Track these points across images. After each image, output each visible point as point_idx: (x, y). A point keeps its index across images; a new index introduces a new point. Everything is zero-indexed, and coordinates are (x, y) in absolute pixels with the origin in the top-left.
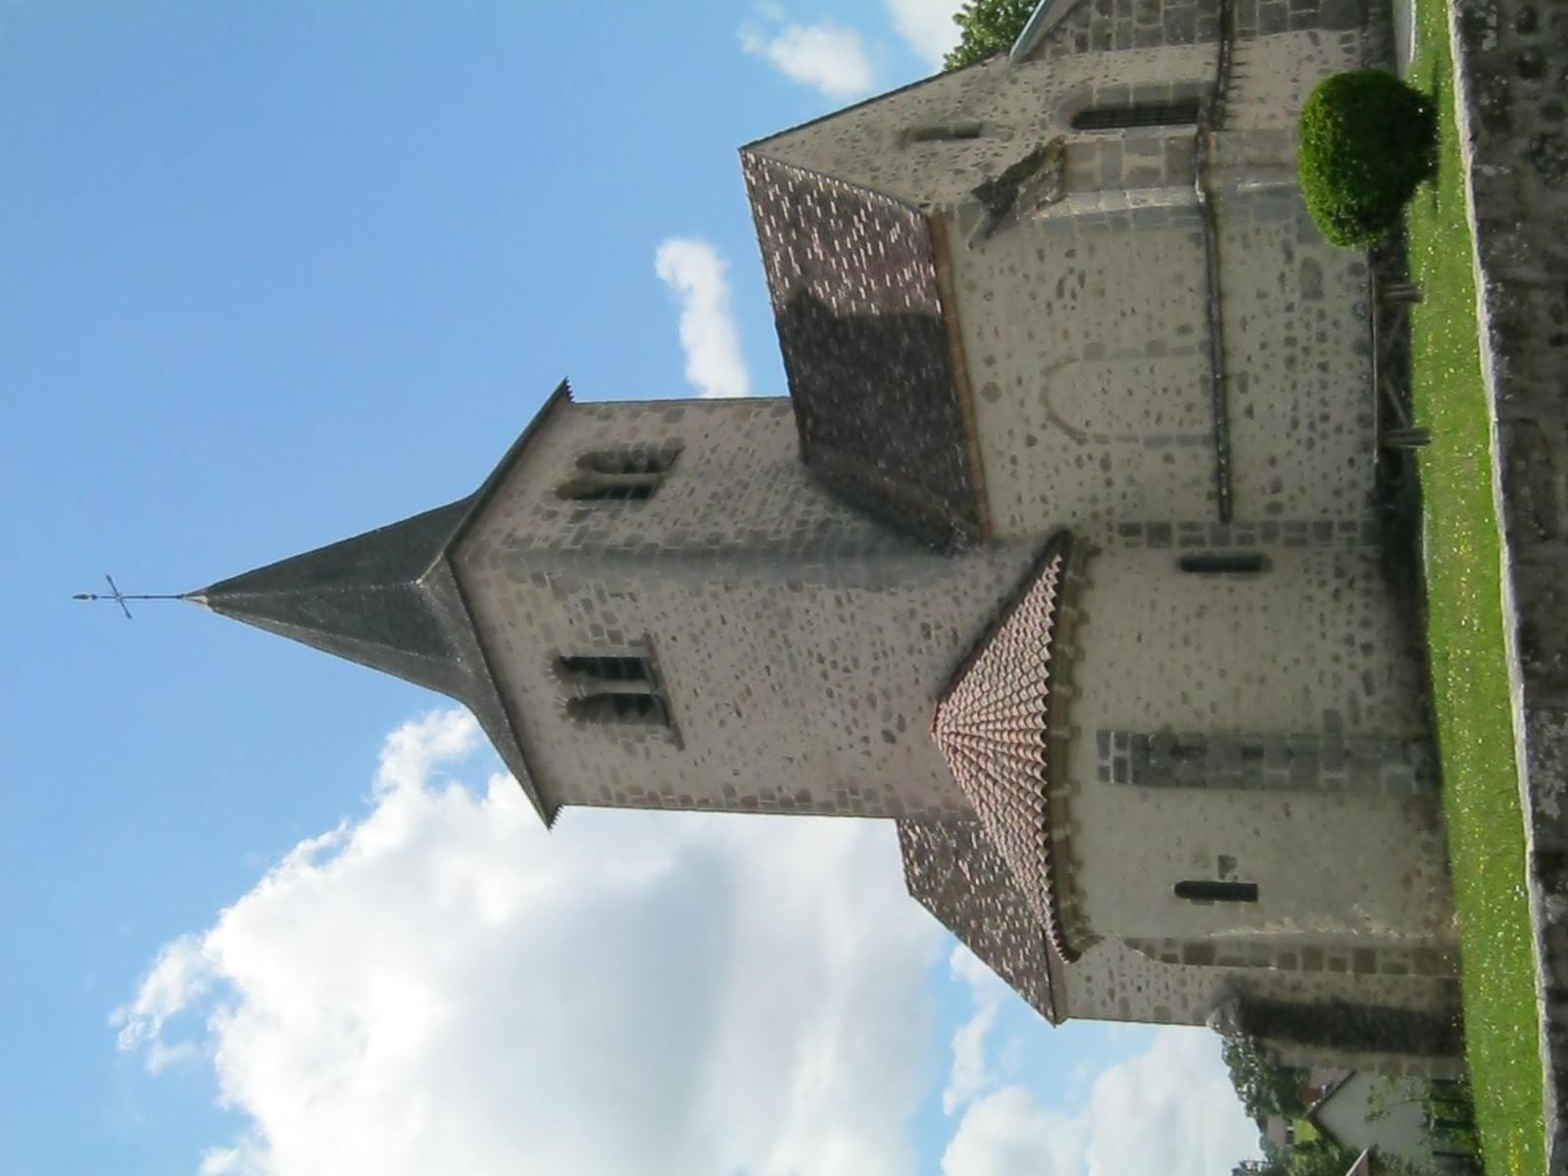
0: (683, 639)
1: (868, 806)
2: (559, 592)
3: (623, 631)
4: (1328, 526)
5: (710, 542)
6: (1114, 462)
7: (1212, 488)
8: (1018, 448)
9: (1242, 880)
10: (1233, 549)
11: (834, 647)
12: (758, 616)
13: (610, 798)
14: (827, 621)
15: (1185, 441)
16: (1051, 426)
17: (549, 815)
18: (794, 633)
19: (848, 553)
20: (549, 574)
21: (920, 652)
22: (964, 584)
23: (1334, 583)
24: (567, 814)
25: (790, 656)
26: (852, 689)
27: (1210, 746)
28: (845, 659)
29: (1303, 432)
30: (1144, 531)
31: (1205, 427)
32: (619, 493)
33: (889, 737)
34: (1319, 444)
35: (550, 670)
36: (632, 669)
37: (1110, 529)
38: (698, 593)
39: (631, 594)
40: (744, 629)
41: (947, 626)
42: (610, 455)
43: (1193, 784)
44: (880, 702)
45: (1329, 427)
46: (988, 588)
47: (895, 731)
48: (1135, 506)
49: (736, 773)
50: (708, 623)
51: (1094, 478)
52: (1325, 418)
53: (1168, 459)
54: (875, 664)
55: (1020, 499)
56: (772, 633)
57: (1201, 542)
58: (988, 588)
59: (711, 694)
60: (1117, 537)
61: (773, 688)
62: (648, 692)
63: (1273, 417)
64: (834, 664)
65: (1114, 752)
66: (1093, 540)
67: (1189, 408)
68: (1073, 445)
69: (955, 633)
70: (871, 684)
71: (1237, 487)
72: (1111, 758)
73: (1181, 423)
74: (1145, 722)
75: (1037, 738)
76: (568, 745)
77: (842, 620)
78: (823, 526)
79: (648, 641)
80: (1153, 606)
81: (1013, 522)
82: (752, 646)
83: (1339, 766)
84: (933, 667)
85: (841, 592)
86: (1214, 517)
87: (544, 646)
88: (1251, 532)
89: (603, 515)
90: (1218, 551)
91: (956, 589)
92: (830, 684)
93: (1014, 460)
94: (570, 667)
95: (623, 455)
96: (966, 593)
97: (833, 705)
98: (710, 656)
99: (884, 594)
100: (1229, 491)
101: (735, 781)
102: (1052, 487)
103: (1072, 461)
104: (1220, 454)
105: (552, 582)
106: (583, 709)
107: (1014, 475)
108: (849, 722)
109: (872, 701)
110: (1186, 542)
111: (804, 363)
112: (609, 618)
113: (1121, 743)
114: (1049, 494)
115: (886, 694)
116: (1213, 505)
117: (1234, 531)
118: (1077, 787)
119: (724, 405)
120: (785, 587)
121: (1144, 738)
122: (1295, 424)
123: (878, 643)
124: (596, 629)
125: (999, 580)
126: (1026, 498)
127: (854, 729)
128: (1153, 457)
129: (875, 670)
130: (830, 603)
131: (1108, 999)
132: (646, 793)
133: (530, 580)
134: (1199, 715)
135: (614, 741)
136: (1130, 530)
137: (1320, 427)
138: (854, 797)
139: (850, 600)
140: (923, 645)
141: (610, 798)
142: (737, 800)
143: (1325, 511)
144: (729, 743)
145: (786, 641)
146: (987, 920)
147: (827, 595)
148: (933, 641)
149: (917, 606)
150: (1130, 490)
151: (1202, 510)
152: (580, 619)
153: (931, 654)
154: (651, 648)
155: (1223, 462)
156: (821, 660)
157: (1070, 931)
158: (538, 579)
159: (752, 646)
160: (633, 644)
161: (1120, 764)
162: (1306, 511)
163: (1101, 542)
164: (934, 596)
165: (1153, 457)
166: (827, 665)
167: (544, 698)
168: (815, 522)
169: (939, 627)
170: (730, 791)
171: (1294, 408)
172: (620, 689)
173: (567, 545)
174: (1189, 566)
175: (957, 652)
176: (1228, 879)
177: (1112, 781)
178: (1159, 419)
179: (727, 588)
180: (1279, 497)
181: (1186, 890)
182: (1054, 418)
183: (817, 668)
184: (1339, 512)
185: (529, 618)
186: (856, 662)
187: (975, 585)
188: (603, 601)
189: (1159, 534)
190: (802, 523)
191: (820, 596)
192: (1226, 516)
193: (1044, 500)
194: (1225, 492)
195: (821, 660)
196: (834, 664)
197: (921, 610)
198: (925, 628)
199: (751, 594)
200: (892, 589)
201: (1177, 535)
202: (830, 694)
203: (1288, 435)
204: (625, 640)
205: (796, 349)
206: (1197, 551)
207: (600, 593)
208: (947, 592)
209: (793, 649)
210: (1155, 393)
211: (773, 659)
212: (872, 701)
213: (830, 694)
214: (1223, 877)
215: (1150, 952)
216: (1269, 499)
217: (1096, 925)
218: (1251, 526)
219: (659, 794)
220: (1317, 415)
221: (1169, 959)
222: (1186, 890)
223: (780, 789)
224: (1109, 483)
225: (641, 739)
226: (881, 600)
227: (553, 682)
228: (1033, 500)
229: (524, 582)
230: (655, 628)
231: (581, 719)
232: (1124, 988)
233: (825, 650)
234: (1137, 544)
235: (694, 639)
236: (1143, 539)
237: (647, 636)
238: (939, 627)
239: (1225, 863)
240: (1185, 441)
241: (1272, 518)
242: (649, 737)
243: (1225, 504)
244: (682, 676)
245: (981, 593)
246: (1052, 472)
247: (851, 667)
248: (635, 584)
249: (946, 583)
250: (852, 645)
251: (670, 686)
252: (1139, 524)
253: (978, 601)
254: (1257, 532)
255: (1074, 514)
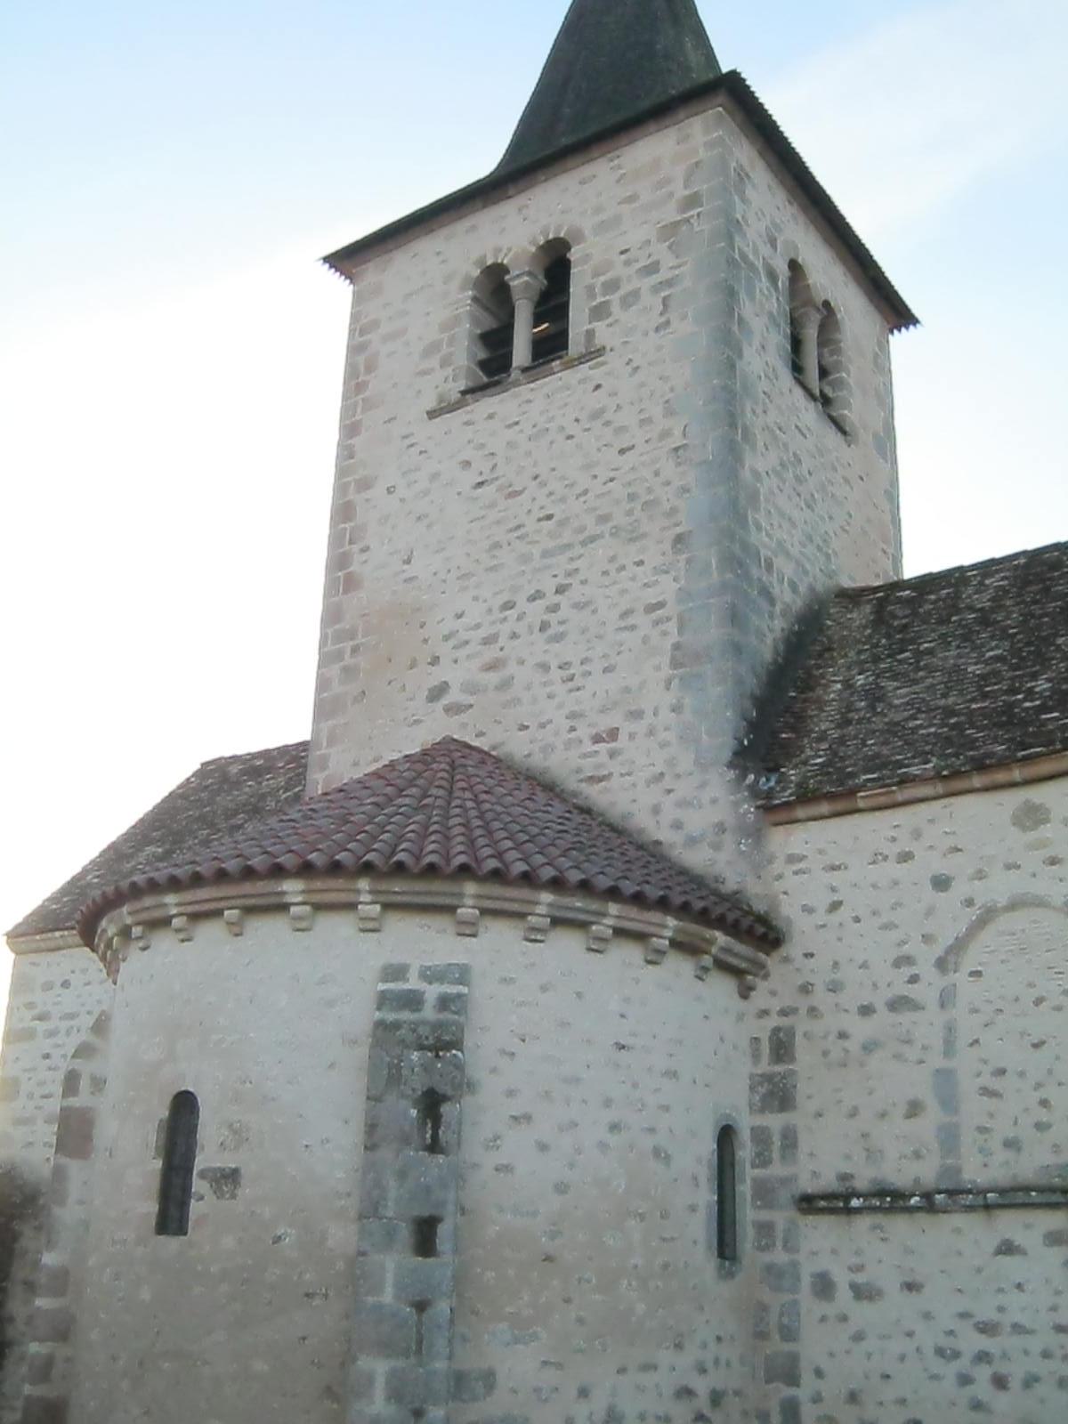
0: (595, 401)
1: (335, 670)
2: (669, 231)
3: (610, 320)
4: (792, 1379)
5: (745, 430)
6: (906, 1018)
7: (861, 1184)
8: (930, 863)
9: (195, 1208)
10: (748, 1214)
11: (579, 606)
12: (632, 497)
13: (361, 335)
14: (624, 592)
15: (949, 1138)
16: (973, 914)
17: (346, 260)
18: (601, 551)
19: (735, 617)
20: (698, 215)
21: (573, 729)
22: (683, 789)
23: (702, 1386)
24: (339, 290)
25: (569, 546)
26: (514, 636)
27: (441, 1158)
28: (561, 623)
29: (972, 1342)
30: (779, 1068)
31: (974, 1172)
32: (796, 343)
33: (438, 692)
34: (950, 1370)
35: (551, 236)
36: (550, 347)
37: (784, 1013)
38: (669, 412)
39: (668, 323)
40: (612, 480)
41: (615, 767)
42: (837, 351)
43: (371, 1128)
44: (493, 678)
45: (982, 1388)
46: (677, 825)
47: (445, 701)
48: (825, 1053)
49: (390, 491)
50: (621, 430)
51: (875, 985)
52: (1000, 1382)
53: (914, 1109)
54: (554, 665)
55: (834, 868)
56: (603, 519)
57: (762, 1160)
58: (677, 825)
59: (511, 445)
60: (774, 1021)
61: (518, 527)
62: (515, 364)
63: (1000, 1290)
64: (554, 609)
65: (432, 992)
66: (762, 986)
67: (1011, 1144)
68: (938, 950)
69: (601, 779)
70: (521, 662)
71: (864, 1222)
72: (422, 986)
73: (982, 1130)
74: (485, 1044)
75: (462, 859)
76: (442, 274)
77: (625, 614)
78: (766, 593)
79: (593, 353)
80: (672, 1074)
81: (792, 859)
82: (586, 492)
83: (396, 1394)
84: (547, 749)
85: (671, 609)
86: (808, 1186)
87: (587, 225)
88: (779, 1244)
89: (773, 305)
90: (745, 1189)
91: (678, 776)
92: (522, 604)
93: (905, 857)
94: (556, 263)
95: (838, 366)
96: (669, 791)
97: (490, 611)
98: (570, 437)
99: (667, 671)
100: (858, 1211)
101: (378, 491)
102: (857, 920)
103: (906, 949)
104: (927, 1196)
105: (687, 220)
106: (494, 286)
107: (878, 858)
108: (463, 636)
109: (491, 667)
110: (761, 1136)
111: (812, 731)
112: (630, 299)
113: (444, 1002)
114: (844, 914)
115: (505, 685)
116: (827, 1181)
117: (781, 1217)
118: (371, 927)
119: (891, 512)
120: (679, 530)
121: (456, 1044)
122: (987, 1329)
123: (586, 668)
124: (612, 286)
125: (692, 841)
126: (835, 878)
127: (452, 642)
128: (919, 1084)
129: (545, 667)
130: (651, 596)
131: (36, 1012)
132: (367, 378)
133: (687, 193)
134: (494, 1142)
135: (444, 327)
136: (782, 1047)
137: (983, 1373)
138: (347, 656)
139: (657, 623)
140: (584, 732)
141: (361, 335)
142: (351, 496)
143: (819, 1373)
144: (435, 476)
145: (593, 539)
146: (160, 850)
147: (667, 588)
148: (589, 747)
149: (649, 719)
150: (853, 1045)
151: (819, 1165)
152: (627, 263)
153: (568, 745)
154: (582, 359)
155: (914, 1201)
156: (560, 590)
157: (125, 914)
158: (692, 201)
159: (586, 492)
160: (590, 334)
161: (412, 1001)
162: (814, 1345)
163: (760, 998)
164: (664, 745)
165: (919, 1084)
166: (553, 599)
167: (512, 233)
168: (771, 583)
169: (612, 754)
170: (365, 485)
171: (1018, 1328)
172: (525, 324)
173: (738, 241)
174: (726, 1136)
175: (572, 784)
176: (198, 1185)
177: (382, 987)
178: (987, 1092)
179: (676, 449)
180: (843, 1294)
181: (184, 1105)
182: (988, 916)
183: (549, 585)
184: (817, 1399)
185: (632, 199)
186: (559, 638)
187: (683, 804)
188: (656, 289)
189: (778, 1095)
190: (769, 566)
191: (665, 580)
192: (808, 1203)
193: (835, 906)
194: (855, 1203)
195: (560, 590)
196: (554, 609)
197: (640, 727)
198: (613, 734)
199: (668, 483)
200: (676, 682)
201: (774, 1122)
202: (509, 605)
203: (964, 1315)
204: (595, 324)
205: (1026, 566)
206: (745, 1152)
207: (669, 283)
208: (671, 762)
209: (578, 550)
210: (1038, 1086)
211: (563, 523)
212: (491, 667)
213: (509, 605)
214: (202, 1175)
215: (84, 1051)
216: (842, 1279)
217: (135, 962)
218: (789, 1246)
219: (367, 394)
220: (1003, 1368)
221: (71, 1083)
222: (184, 1105)
223: (365, 550)
224: (866, 1011)
225: (444, 363)
226: (658, 668)
227: (533, 242)
228: (833, 890)
229: (687, 183)
230: (613, 361)
231: (477, 284)
232: (52, 1034)
233: (576, 593)
234: (756, 1056)
235: (596, 415)
236: (765, 1066)
237: (600, 351)
238: (612, 754)
239: (228, 1179)
240: (949, 1138)
241: (806, 1281)
242: (449, 371)
243: (831, 1203)
244: (535, 402)
245: (670, 813)
246: (884, 920)
247: (551, 632)
248: (683, 327)
249: (686, 762)
250: (583, 632)
251: (524, 391)
252: (792, 1059)
253: (656, 810)
254: (779, 1257)
255: (809, 955)
